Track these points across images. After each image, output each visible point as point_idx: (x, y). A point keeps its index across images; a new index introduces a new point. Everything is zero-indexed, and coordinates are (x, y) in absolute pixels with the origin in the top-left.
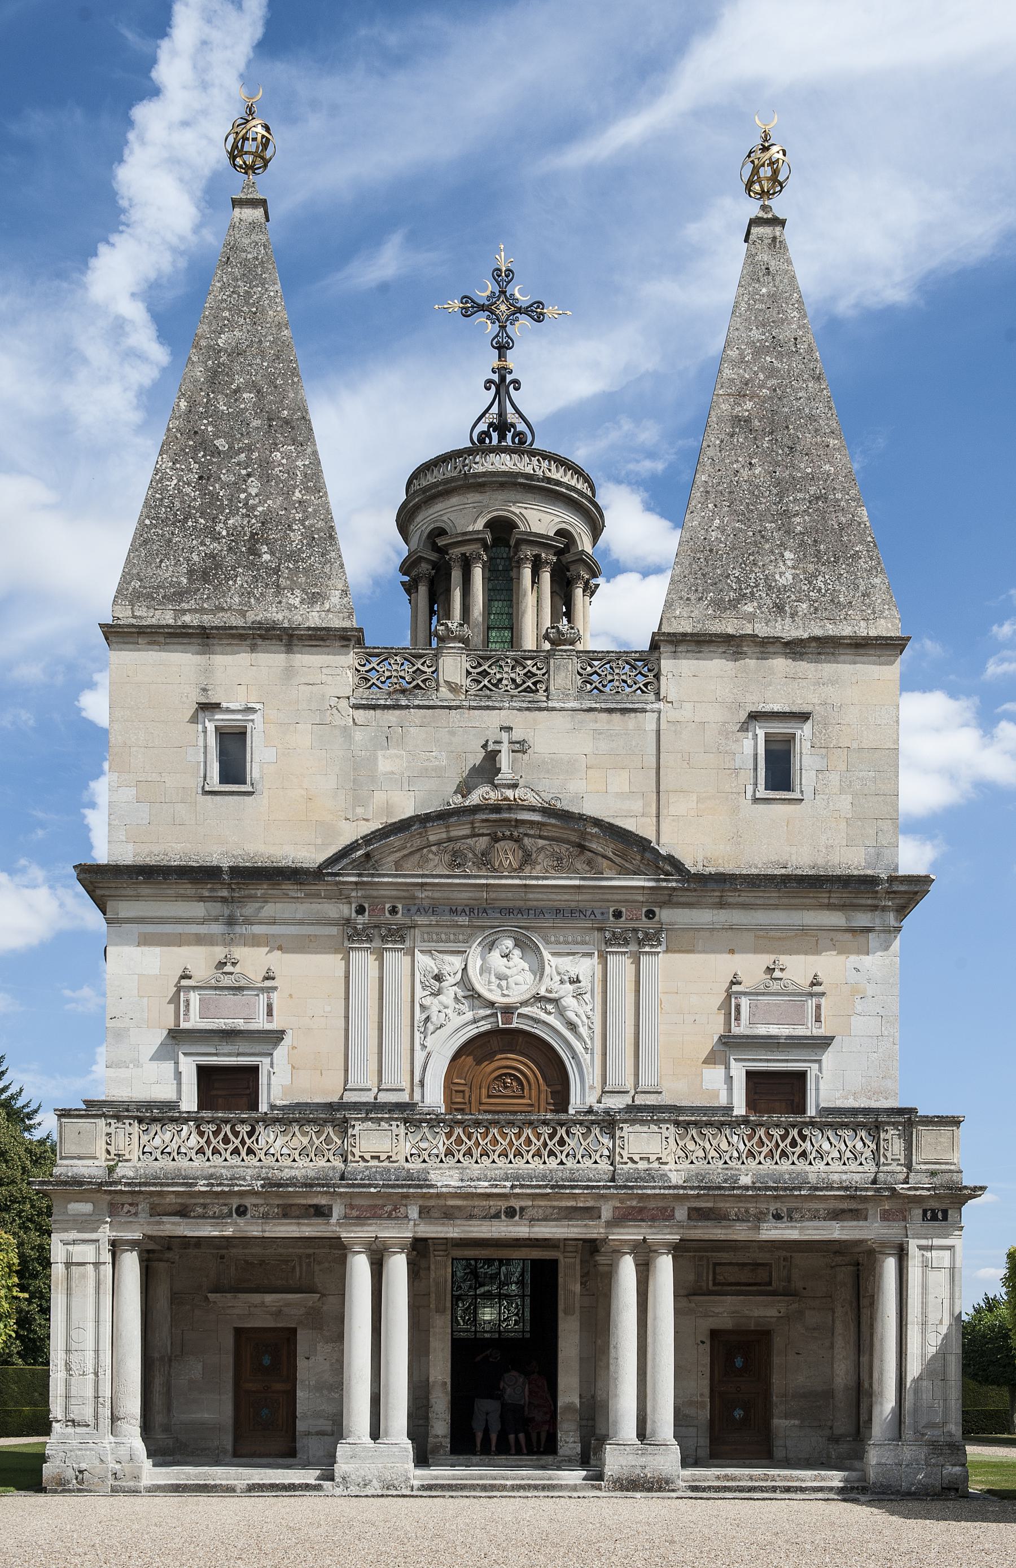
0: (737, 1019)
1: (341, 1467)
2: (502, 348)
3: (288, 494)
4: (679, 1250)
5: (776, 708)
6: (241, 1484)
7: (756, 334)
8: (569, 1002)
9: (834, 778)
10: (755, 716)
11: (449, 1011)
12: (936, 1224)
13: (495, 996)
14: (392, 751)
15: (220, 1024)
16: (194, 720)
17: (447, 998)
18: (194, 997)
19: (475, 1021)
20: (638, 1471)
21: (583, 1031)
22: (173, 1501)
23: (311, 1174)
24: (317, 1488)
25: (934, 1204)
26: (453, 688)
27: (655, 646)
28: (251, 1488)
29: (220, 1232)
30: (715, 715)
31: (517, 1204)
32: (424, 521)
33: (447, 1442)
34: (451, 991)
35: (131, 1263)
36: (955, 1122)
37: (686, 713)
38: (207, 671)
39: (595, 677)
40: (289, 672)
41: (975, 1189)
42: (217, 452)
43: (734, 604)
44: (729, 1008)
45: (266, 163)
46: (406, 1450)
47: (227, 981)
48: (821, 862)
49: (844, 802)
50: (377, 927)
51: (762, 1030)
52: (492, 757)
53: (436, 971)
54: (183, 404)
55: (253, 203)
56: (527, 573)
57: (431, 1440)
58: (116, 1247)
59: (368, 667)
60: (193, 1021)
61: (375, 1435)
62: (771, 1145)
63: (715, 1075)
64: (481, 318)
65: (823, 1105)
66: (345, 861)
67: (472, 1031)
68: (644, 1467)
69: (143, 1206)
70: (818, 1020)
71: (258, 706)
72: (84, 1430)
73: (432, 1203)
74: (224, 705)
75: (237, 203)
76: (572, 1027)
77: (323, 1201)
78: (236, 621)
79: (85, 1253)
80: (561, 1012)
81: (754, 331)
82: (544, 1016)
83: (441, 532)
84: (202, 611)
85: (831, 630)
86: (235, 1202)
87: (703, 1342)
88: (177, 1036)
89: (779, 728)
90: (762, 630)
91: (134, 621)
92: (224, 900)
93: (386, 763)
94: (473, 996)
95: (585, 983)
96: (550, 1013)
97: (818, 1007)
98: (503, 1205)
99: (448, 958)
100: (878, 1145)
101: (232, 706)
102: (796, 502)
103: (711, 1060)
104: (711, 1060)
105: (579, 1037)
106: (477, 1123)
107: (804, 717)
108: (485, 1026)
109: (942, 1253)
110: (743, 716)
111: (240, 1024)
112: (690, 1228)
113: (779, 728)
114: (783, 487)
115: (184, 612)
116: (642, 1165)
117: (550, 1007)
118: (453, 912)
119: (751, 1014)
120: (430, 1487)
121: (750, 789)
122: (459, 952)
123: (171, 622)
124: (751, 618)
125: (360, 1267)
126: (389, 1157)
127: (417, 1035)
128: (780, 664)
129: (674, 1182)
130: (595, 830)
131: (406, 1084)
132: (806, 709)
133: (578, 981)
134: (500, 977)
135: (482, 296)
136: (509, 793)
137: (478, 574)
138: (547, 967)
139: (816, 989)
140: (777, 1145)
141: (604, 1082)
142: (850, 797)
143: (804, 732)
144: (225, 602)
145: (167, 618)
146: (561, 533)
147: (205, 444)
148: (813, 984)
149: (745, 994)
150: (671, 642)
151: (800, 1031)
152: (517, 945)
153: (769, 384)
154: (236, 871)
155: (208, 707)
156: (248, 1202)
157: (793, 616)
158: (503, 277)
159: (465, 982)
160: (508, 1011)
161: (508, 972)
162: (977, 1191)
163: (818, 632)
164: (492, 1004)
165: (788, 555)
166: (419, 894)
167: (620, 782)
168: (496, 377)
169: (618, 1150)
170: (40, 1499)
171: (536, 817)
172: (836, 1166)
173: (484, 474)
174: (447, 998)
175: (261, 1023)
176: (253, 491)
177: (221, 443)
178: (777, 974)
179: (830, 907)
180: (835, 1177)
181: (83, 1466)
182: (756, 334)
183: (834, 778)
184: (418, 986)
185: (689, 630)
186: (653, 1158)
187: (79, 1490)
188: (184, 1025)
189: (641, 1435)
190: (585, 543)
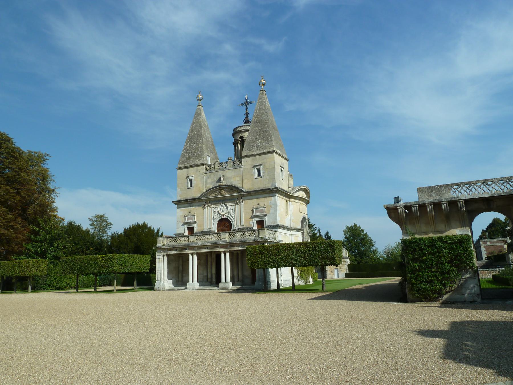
0: (254, 213)
1: (187, 287)
2: (247, 109)
3: (199, 146)
4: (230, 252)
5: (258, 164)
6: (176, 289)
7: (259, 108)
8: (231, 213)
9: (266, 173)
10: (255, 166)
11: (216, 216)
14: (209, 179)
15: (189, 221)
16: (186, 178)
17: (216, 214)
18: (186, 218)
19: (219, 217)
20: (223, 287)
21: (233, 217)
23: (185, 244)
24: (185, 290)
25: (262, 242)
26: (217, 169)
28: (177, 290)
29: (435, 232)
30: (249, 167)
31: (208, 246)
34: (217, 213)
35: (166, 258)
37: (246, 167)
38: (188, 172)
40: (197, 170)
42: (191, 141)
43: (251, 150)
44: (253, 212)
46: (276, 286)
47: (190, 215)
48: (265, 187)
49: (268, 177)
51: (257, 214)
52: (220, 179)
54: (188, 135)
57: (213, 282)
58: (164, 256)
60: (186, 221)
61: (193, 282)
63: (251, 222)
65: (266, 225)
66: (202, 196)
67: (219, 219)
68: (224, 286)
69: (166, 250)
71: (193, 176)
72: (159, 282)
73: (198, 247)
75: (198, 106)
76: (232, 217)
77: (186, 248)
78: (191, 165)
79: (160, 257)
80: (230, 215)
81: (259, 107)
84: (187, 164)
85: (264, 151)
86: (176, 249)
88: (184, 224)
89: (258, 167)
90: (255, 153)
91: (180, 167)
92: (189, 203)
93: (209, 181)
94: (219, 214)
95: (233, 210)
97: (265, 210)
98: (207, 247)
102: (262, 132)
103: (250, 219)
104: (250, 219)
105: (233, 218)
106: (204, 235)
107: (261, 165)
108: (221, 218)
109: (159, 256)
110: (253, 166)
111: (191, 221)
113: (258, 167)
114: (260, 130)
115: (185, 164)
116: (224, 239)
117: (229, 214)
118: (216, 201)
121: (254, 177)
123: (184, 166)
124: (254, 151)
127: (213, 220)
128: (258, 157)
129: (228, 242)
130: (232, 187)
131: (211, 228)
134: (223, 210)
136: (222, 183)
138: (228, 208)
141: (236, 225)
142: (268, 176)
145: (183, 166)
147: (190, 141)
150: (243, 157)
151: (263, 214)
153: (260, 115)
154: (189, 199)
155: (188, 177)
156: (177, 249)
157: (259, 150)
158: (247, 99)
159: (218, 212)
160: (223, 215)
161: (223, 209)
163: (263, 152)
164: (221, 214)
165: (260, 141)
166: (212, 199)
167: (237, 179)
170: (154, 291)
171: (225, 186)
172: (250, 237)
173: (239, 130)
174: (216, 214)
175: (194, 221)
176: (195, 146)
177: (192, 140)
178: (259, 205)
179: (266, 194)
180: (249, 239)
181: (159, 287)
182: (259, 108)
183: (266, 173)
184: (213, 213)
185: (246, 155)
186: (225, 238)
187: (158, 290)
188: (185, 222)
189: (225, 281)
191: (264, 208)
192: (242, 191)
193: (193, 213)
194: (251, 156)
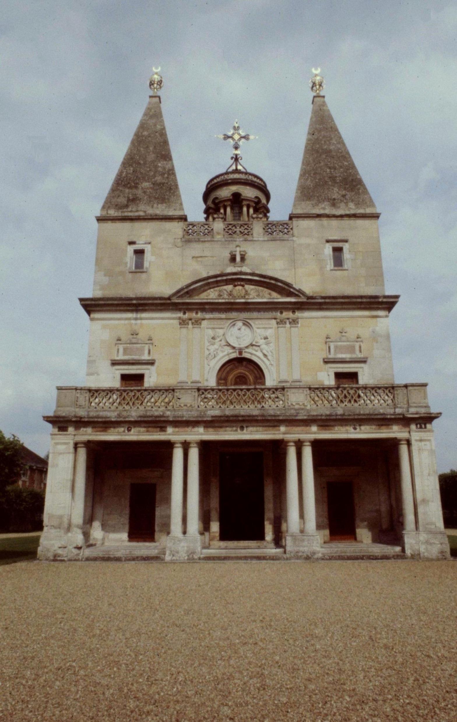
8: (264, 346)
12: (422, 430)
13: (236, 345)
19: (228, 354)
21: (269, 357)
22: (210, 565)
27: (291, 218)
32: (213, 196)
33: (218, 535)
35: (82, 453)
36: (425, 385)
39: (269, 230)
41: (438, 414)
45: (161, 87)
47: (134, 341)
50: (190, 319)
53: (213, 335)
55: (155, 97)
56: (245, 209)
58: (76, 446)
59: (189, 228)
62: (350, 397)
64: (230, 140)
70: (360, 351)
74: (137, 242)
82: (254, 352)
83: (216, 198)
87: (324, 488)
96: (257, 351)
97: (360, 347)
99: (218, 330)
100: (394, 397)
101: (141, 242)
107: (346, 241)
112: (318, 433)
117: (257, 348)
119: (335, 351)
120: (331, 558)
122: (221, 328)
125: (178, 454)
126: (191, 405)
132: (345, 238)
133: (267, 338)
135: (230, 134)
137: (228, 210)
139: (359, 339)
140: (352, 397)
143: (346, 247)
144: (139, 209)
146: (256, 197)
148: (358, 338)
149: (331, 342)
151: (354, 356)
152: (244, 324)
162: (437, 416)
168: (235, 156)
169: (286, 401)
175: (146, 357)
186: (301, 403)
190: (264, 201)
191: (357, 342)
192: (299, 293)
193: (143, 335)
194: (319, 216)
